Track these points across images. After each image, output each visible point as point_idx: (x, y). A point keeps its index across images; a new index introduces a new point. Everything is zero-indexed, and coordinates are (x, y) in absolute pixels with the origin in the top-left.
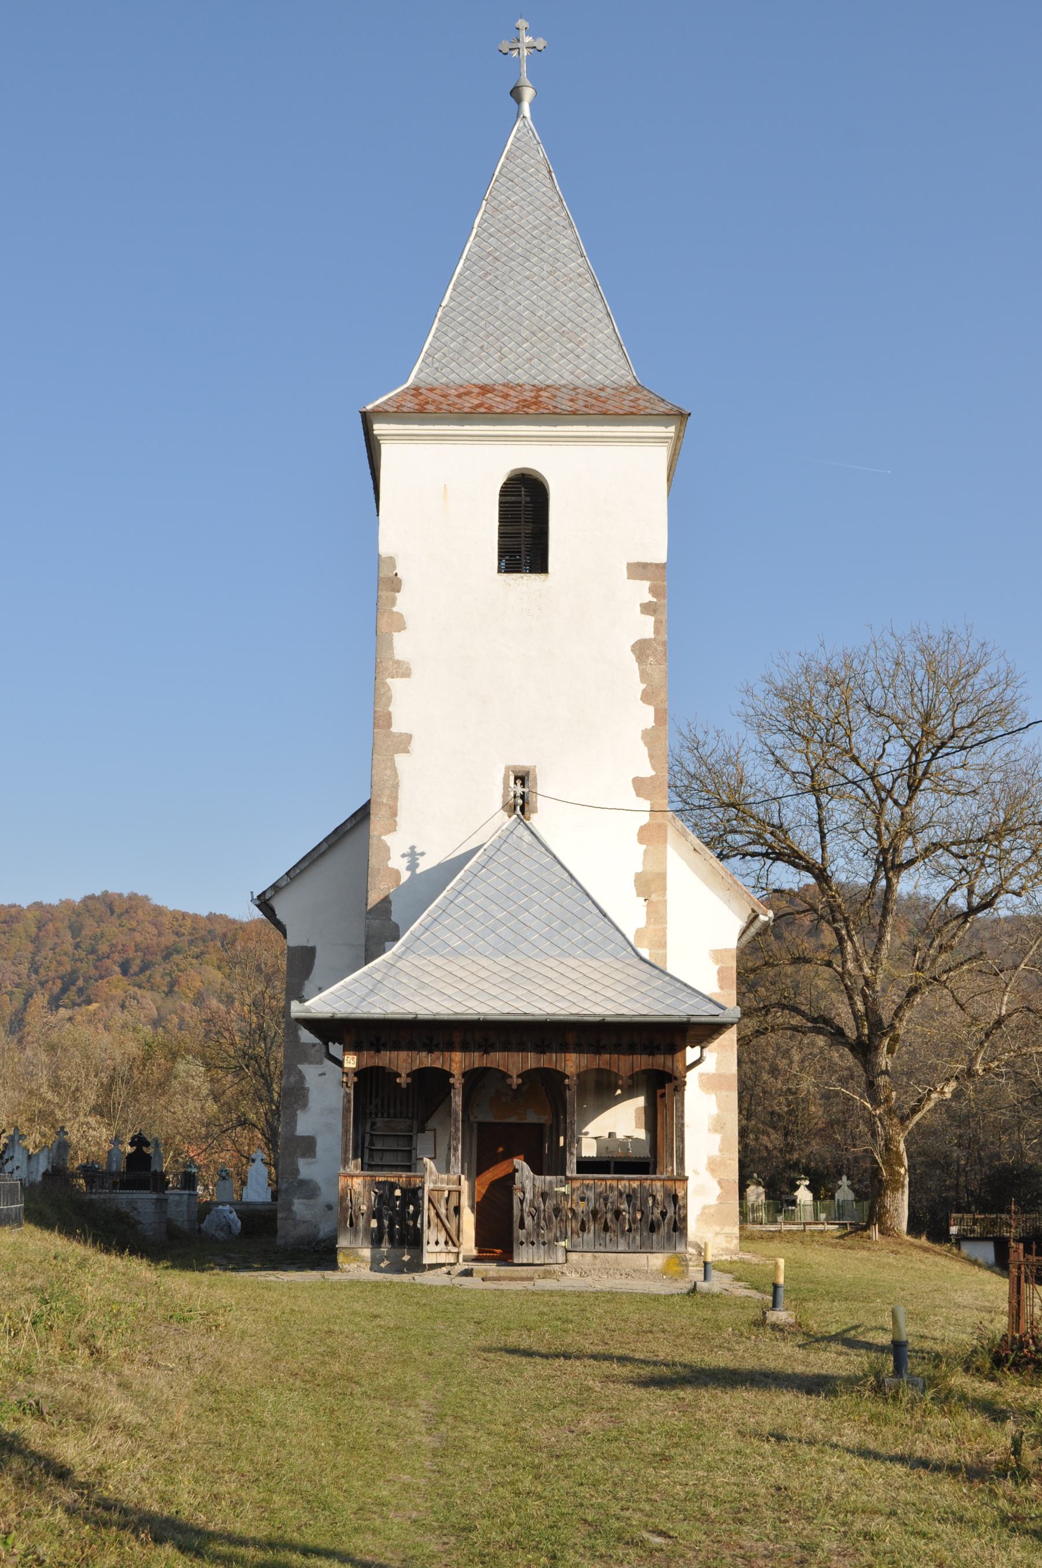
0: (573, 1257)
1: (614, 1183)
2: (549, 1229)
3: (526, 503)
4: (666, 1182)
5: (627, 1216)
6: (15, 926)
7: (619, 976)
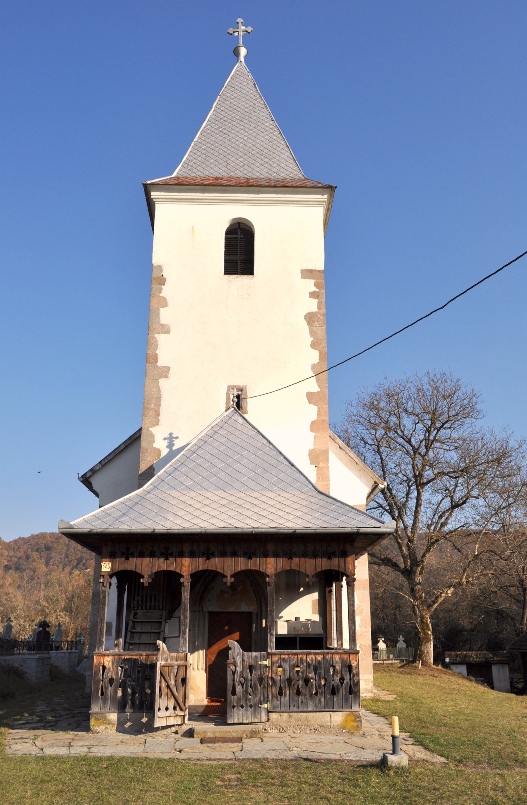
1: (304, 657)
2: (255, 694)
3: (241, 238)
4: (343, 656)
5: (314, 683)
6: (60, 540)
7: (304, 503)
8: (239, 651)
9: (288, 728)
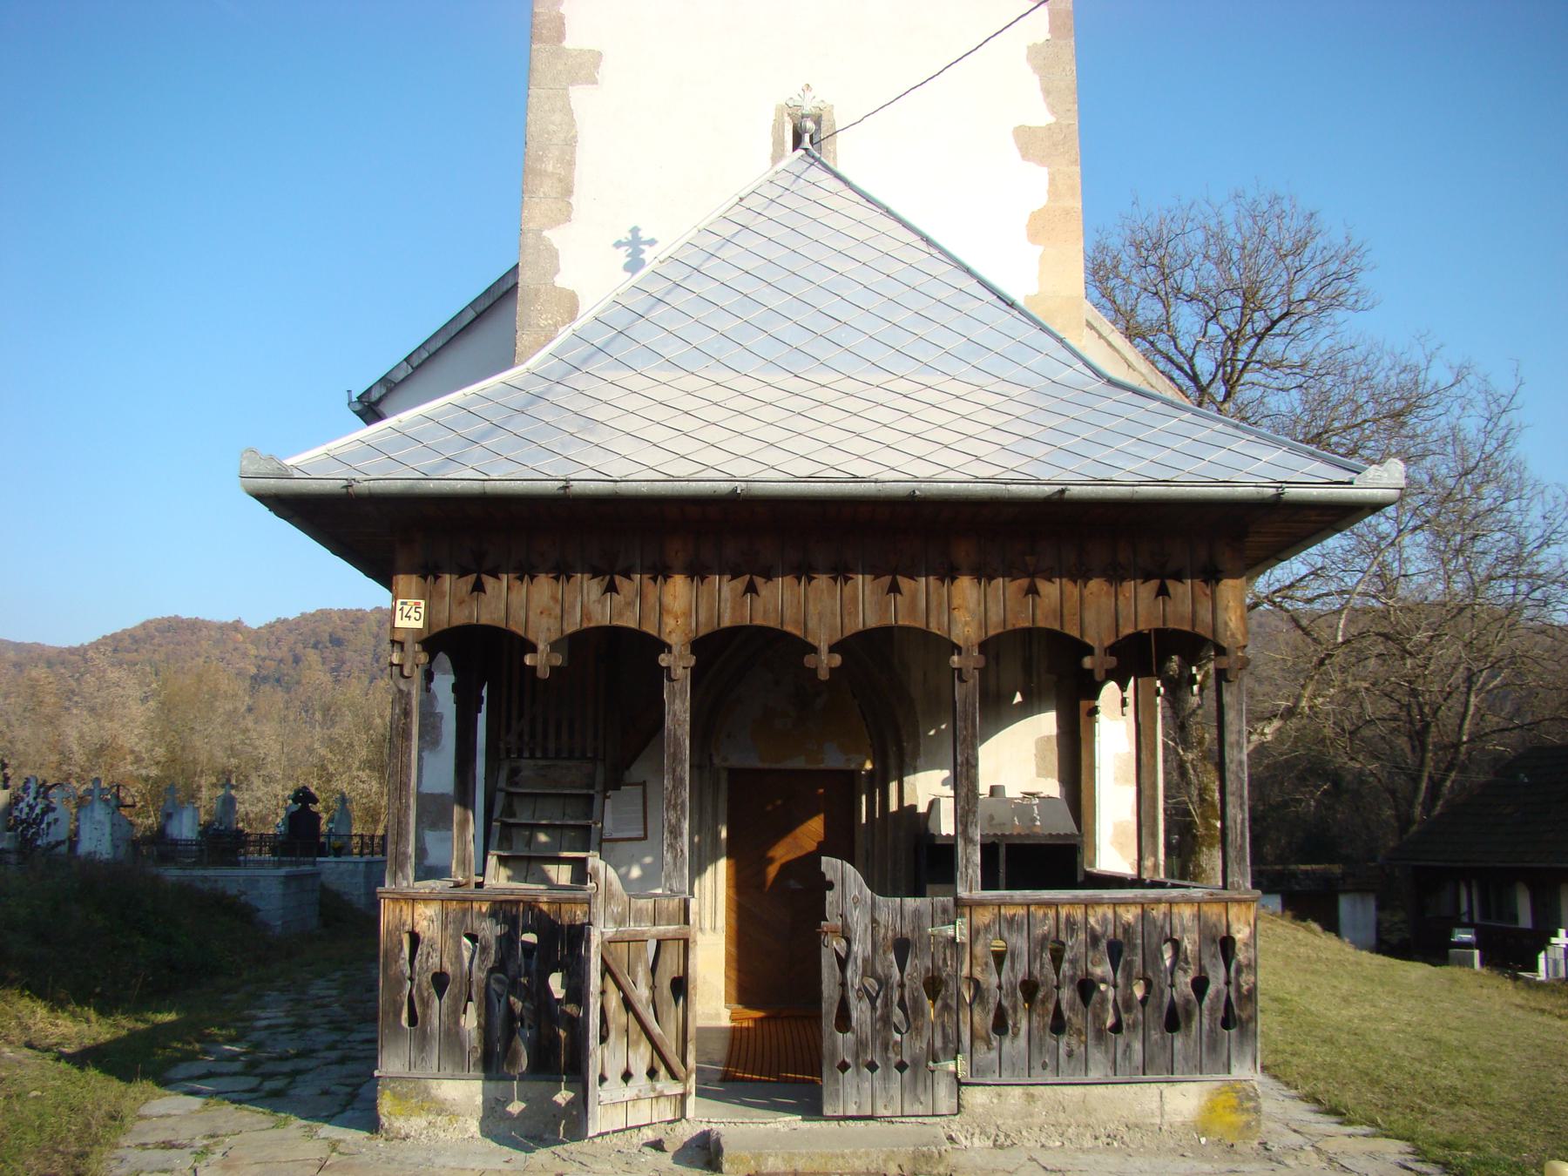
0: (977, 1098)
4: (1205, 908)
8: (860, 893)
9: (1024, 1133)
